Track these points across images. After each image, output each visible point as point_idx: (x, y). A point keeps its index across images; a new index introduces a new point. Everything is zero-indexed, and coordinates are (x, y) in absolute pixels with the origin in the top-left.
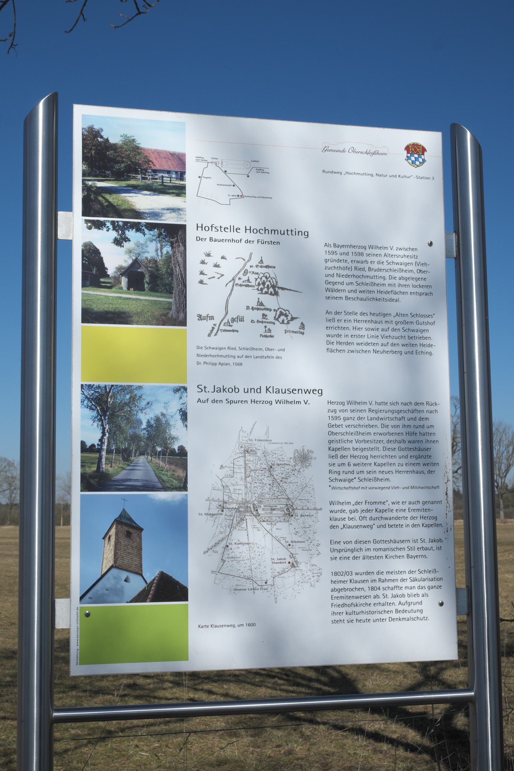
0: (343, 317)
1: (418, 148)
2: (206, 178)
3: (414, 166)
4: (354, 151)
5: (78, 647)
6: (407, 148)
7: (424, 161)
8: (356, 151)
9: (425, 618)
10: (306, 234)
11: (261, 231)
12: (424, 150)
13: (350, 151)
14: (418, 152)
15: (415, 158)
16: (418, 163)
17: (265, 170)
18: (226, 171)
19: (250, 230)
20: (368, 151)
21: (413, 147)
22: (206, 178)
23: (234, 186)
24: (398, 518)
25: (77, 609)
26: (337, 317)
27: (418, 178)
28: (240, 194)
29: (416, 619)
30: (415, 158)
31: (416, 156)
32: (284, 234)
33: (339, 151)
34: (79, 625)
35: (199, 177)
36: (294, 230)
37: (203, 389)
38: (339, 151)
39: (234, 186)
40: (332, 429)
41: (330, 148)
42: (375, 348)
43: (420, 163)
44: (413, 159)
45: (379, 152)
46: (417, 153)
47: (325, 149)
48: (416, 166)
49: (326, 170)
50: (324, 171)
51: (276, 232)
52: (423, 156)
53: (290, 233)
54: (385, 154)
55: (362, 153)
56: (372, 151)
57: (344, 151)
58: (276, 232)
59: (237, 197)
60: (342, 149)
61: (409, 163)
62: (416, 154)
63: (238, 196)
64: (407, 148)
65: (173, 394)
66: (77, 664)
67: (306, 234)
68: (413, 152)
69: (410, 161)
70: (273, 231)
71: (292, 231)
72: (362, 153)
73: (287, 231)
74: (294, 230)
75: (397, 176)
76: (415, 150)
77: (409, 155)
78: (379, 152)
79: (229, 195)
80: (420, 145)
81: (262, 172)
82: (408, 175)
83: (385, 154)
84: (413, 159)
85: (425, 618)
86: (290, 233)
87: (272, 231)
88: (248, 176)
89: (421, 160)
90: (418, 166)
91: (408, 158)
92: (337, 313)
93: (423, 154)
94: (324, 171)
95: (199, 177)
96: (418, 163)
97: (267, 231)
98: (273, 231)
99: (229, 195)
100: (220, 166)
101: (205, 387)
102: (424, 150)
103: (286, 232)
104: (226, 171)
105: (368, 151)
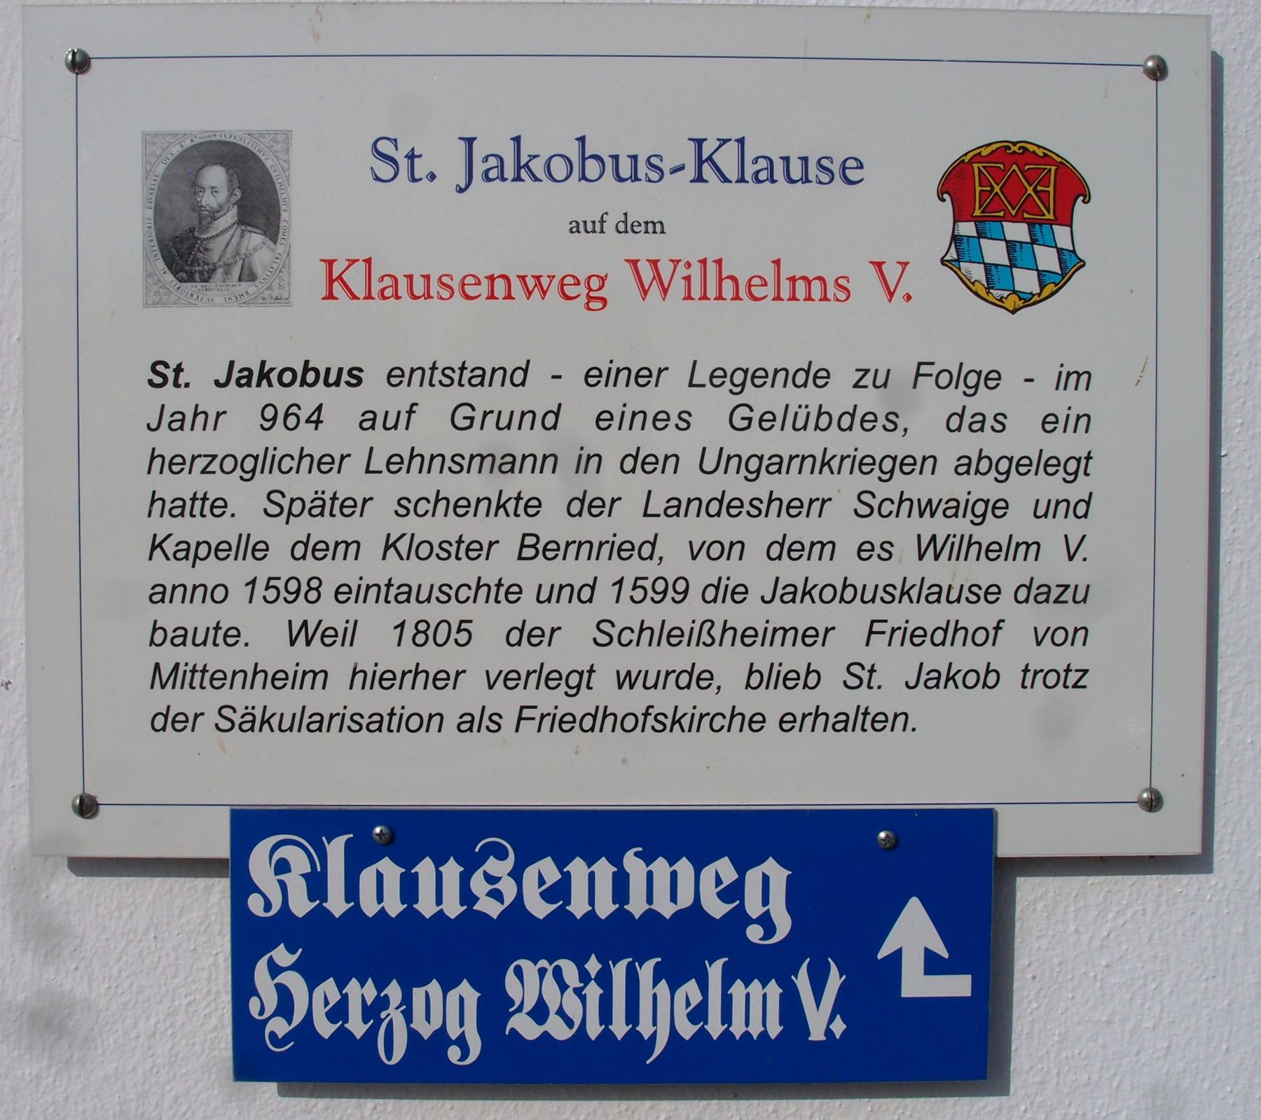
3: (999, 303)
6: (958, 184)
7: (1070, 263)
9: (1073, 677)
15: (1011, 246)
21: (997, 174)
24: (510, 464)
30: (1011, 246)
31: (1017, 231)
37: (404, 164)
44: (995, 252)
48: (1012, 301)
52: (1061, 233)
61: (968, 283)
64: (958, 184)
65: (90, 791)
69: (977, 272)
77: (968, 229)
85: (1073, 677)
89: (1047, 259)
90: (1028, 301)
91: (959, 253)
96: (1026, 281)
101: (411, 157)
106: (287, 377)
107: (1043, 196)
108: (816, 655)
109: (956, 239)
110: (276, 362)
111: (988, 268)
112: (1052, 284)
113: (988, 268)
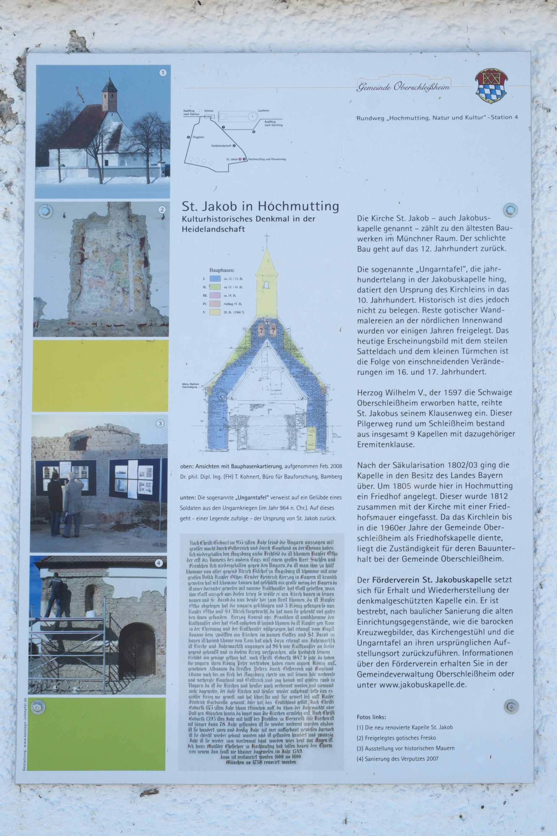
0: (387, 554)
1: (495, 76)
2: (198, 138)
3: (488, 102)
4: (402, 87)
5: (26, 749)
6: (479, 78)
7: (503, 93)
8: (405, 86)
9: (429, 476)
10: (336, 207)
11: (278, 207)
12: (504, 77)
13: (397, 87)
14: (495, 81)
15: (491, 90)
16: (494, 97)
17: (278, 122)
18: (223, 127)
19: (265, 206)
20: (422, 86)
21: (488, 75)
22: (198, 138)
23: (234, 146)
25: (25, 701)
26: (383, 471)
27: (494, 117)
28: (243, 156)
29: (459, 675)
30: (491, 90)
31: (492, 87)
32: (307, 209)
33: (381, 88)
34: (27, 721)
35: (188, 137)
36: (321, 203)
37: (190, 207)
38: (381, 88)
39: (234, 146)
40: (363, 398)
41: (367, 86)
42: (468, 480)
43: (498, 96)
44: (487, 91)
45: (438, 86)
46: (494, 83)
47: (361, 87)
48: (491, 101)
49: (362, 116)
50: (358, 118)
51: (298, 206)
52: (502, 87)
53: (314, 207)
54: (447, 88)
55: (413, 88)
56: (428, 85)
57: (387, 88)
58: (298, 206)
59: (238, 161)
60: (384, 86)
62: (492, 84)
63: (240, 159)
64: (479, 78)
66: (24, 770)
67: (336, 207)
68: (487, 81)
69: (483, 95)
70: (294, 206)
71: (317, 204)
72: (413, 88)
73: (312, 204)
74: (321, 203)
75: (464, 117)
76: (491, 78)
77: (481, 86)
78: (438, 86)
79: (228, 159)
80: (499, 72)
81: (273, 125)
82: (479, 115)
83: (447, 88)
84: (487, 91)
85: (429, 476)
86: (314, 207)
87: (292, 206)
88: (254, 132)
89: (498, 92)
90: (494, 101)
91: (480, 91)
92: (382, 466)
93: (502, 84)
94: (358, 118)
95: (188, 137)
97: (286, 206)
98: (294, 206)
99: (228, 159)
100: (216, 120)
101: (192, 205)
102: (504, 77)
103: (310, 206)
104: (223, 127)
105: (422, 86)
106: (226, 208)
107: (498, 79)
108: (223, 738)
109: (479, 89)
110: (221, 203)
111: (486, 95)
112: (500, 97)
113: (486, 95)
